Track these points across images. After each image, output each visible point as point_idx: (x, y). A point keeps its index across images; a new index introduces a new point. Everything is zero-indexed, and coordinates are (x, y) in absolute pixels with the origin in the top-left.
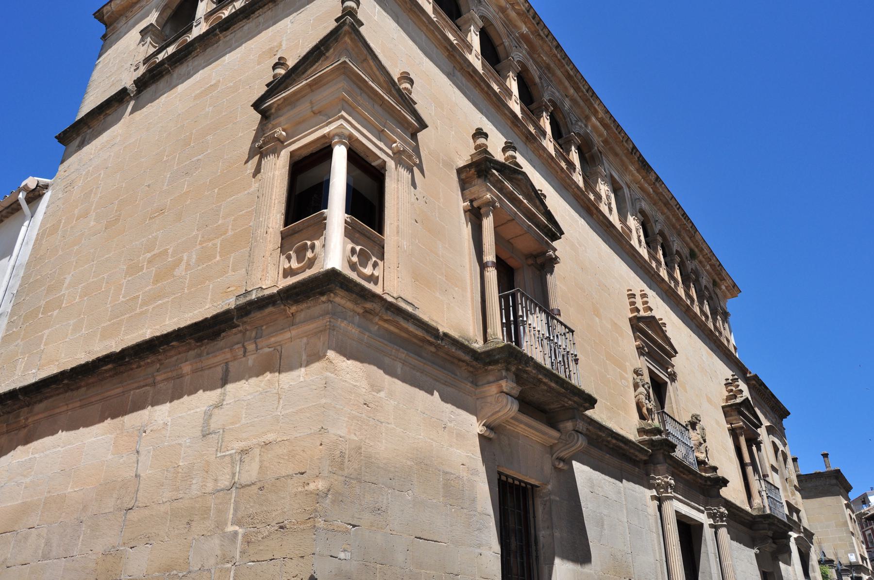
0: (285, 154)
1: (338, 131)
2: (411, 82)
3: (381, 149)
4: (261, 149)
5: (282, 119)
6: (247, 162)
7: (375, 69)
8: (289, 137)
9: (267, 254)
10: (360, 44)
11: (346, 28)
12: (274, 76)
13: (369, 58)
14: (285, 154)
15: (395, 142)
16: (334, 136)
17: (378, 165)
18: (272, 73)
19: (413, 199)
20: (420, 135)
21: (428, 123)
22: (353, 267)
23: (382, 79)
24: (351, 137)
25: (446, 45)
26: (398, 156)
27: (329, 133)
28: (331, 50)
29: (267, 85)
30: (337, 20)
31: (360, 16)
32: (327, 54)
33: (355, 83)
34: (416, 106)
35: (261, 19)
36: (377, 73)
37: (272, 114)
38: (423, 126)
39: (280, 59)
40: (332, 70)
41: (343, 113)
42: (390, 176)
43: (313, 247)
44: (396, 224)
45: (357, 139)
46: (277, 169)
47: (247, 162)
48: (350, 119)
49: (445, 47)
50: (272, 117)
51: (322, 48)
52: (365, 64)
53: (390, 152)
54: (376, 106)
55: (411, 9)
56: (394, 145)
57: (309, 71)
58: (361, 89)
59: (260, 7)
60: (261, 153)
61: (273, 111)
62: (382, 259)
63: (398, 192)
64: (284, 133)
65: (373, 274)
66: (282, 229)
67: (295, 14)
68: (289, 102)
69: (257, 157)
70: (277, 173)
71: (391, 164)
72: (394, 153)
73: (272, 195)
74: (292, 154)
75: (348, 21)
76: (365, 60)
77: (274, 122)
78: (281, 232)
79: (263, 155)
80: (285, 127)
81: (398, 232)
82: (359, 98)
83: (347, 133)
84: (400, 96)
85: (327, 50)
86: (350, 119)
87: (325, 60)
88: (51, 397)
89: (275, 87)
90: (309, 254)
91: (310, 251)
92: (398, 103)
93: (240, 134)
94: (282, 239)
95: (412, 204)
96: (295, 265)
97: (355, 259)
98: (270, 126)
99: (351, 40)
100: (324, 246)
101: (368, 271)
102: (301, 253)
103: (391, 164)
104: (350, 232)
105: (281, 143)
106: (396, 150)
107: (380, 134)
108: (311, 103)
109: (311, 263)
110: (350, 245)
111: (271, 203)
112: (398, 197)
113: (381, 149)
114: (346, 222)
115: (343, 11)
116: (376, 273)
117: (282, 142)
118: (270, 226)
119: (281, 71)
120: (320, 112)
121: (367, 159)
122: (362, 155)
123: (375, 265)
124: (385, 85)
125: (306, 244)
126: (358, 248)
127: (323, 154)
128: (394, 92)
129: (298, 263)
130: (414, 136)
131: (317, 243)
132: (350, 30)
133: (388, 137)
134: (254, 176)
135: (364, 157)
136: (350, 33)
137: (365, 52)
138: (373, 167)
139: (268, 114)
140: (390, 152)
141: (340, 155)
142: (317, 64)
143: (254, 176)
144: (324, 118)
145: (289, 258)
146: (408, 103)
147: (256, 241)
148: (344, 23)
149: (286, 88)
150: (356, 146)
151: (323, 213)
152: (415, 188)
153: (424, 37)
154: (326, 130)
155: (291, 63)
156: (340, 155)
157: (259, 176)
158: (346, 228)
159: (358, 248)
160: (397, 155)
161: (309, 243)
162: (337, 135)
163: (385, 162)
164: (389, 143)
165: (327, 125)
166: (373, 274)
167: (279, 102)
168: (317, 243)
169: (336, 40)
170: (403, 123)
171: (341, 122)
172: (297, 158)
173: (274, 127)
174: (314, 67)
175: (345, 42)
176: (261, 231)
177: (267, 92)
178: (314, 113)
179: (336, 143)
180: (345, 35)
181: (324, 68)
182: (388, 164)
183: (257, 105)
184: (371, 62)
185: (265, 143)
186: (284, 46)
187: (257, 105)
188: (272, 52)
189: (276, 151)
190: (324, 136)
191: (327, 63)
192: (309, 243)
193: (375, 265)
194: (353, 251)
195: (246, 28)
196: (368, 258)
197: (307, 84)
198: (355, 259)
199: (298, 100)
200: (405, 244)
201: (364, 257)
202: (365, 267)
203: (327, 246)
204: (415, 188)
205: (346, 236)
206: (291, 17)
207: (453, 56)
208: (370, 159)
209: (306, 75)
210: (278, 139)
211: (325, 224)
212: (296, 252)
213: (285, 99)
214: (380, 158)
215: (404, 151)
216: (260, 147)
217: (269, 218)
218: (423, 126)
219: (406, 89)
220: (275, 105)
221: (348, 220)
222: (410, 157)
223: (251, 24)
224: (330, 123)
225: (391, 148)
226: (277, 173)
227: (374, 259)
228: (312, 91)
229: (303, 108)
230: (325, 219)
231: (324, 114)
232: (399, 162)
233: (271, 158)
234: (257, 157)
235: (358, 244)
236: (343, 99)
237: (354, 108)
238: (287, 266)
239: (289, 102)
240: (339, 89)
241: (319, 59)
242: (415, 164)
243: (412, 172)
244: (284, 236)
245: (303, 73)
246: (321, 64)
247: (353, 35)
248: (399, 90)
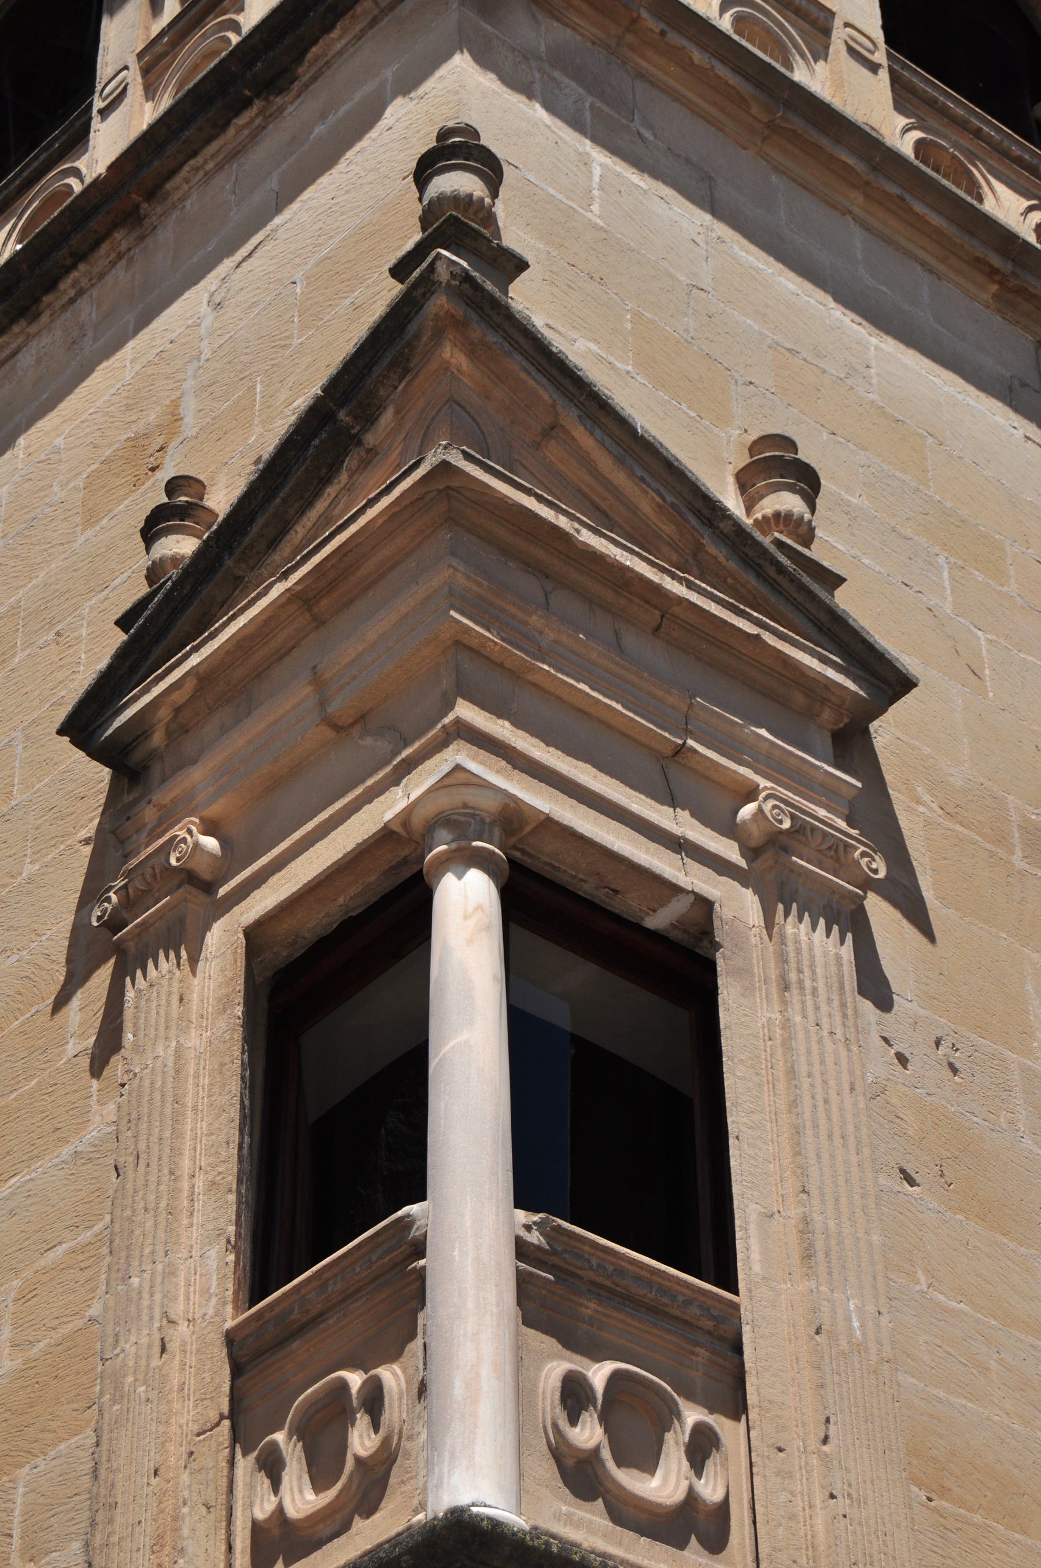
0: (223, 940)
1: (444, 801)
2: (807, 481)
3: (678, 845)
4: (123, 927)
5: (197, 775)
6: (61, 1001)
7: (605, 463)
8: (235, 853)
9: (175, 1455)
10: (516, 364)
11: (439, 303)
12: (153, 574)
13: (570, 418)
14: (223, 940)
15: (750, 794)
16: (431, 827)
17: (679, 924)
18: (143, 561)
19: (879, 1064)
20: (885, 732)
21: (909, 662)
22: (581, 1476)
23: (647, 503)
24: (512, 819)
25: (979, 250)
26: (773, 864)
27: (406, 817)
28: (387, 418)
29: (124, 623)
30: (399, 271)
31: (514, 236)
32: (370, 439)
33: (505, 551)
34: (843, 599)
35: (87, 310)
36: (620, 478)
37: (154, 755)
38: (890, 683)
39: (173, 486)
40: (392, 514)
41: (465, 711)
42: (743, 972)
43: (374, 1399)
44: (794, 1212)
45: (548, 823)
46: (196, 1012)
47: (61, 1001)
48: (502, 729)
49: (978, 262)
50: (156, 771)
51: (342, 415)
52: (553, 451)
53: (729, 850)
54: (631, 640)
55: (770, 125)
56: (747, 811)
57: (299, 531)
58: (543, 573)
59: (80, 257)
60: (119, 950)
61: (157, 739)
62: (736, 1406)
63: (787, 1043)
64: (210, 843)
65: (692, 1497)
66: (229, 1324)
67: (228, 263)
68: (227, 689)
69: (104, 974)
70: (194, 1041)
71: (738, 906)
72: (751, 852)
73: (176, 1152)
74: (255, 936)
75: (442, 273)
76: (552, 430)
77: (164, 796)
78: (230, 1339)
79: (130, 963)
80: (214, 810)
81: (808, 1255)
82: (535, 620)
83: (488, 804)
84: (747, 562)
85: (368, 417)
86: (502, 729)
87: (365, 464)
88: (361, 1557)
89: (155, 628)
90: (362, 1441)
91: (362, 1420)
92: (743, 599)
93: (29, 869)
94: (237, 1370)
95: (877, 1092)
96: (301, 1499)
97: (588, 1433)
98: (149, 814)
99: (472, 351)
100: (422, 1389)
101: (663, 1484)
102: (323, 1431)
103: (738, 906)
104: (548, 1297)
105: (202, 890)
106: (756, 836)
107: (668, 775)
108: (318, 681)
109: (372, 1484)
110: (556, 1366)
111: (174, 1193)
112: (792, 1072)
113: (678, 845)
114: (522, 1250)
115: (425, 221)
116: (710, 1490)
117: (209, 887)
118: (178, 1309)
119: (181, 546)
120: (362, 718)
121: (616, 905)
122: (587, 889)
123: (701, 1448)
124: (667, 529)
125: (343, 1386)
126: (599, 1375)
127: (392, 918)
128: (716, 551)
129: (317, 1489)
130: (851, 744)
131: (391, 1376)
132: (459, 310)
133: (708, 774)
134: (98, 1063)
135: (601, 896)
136: (460, 325)
137: (546, 393)
138: (654, 935)
139: (137, 755)
140: (729, 850)
141: (466, 908)
142: (331, 491)
143: (98, 1063)
144: (383, 745)
145: (272, 1467)
146: (794, 586)
147: (119, 1395)
148: (427, 285)
149: (202, 626)
150: (546, 855)
151: (406, 1224)
152: (884, 1001)
153: (858, 239)
154: (391, 806)
155: (220, 500)
156: (466, 908)
157: (116, 1066)
158: (522, 1281)
159: (599, 1375)
160: (766, 860)
161: (355, 1379)
162: (445, 820)
163: (705, 905)
164: (717, 804)
165: (396, 779)
166: (692, 1497)
167: (179, 697)
168: (391, 1376)
169: (403, 367)
170: (783, 695)
171: (460, 755)
172: (281, 954)
173: (168, 818)
174: (320, 506)
175: (446, 367)
176: (138, 1341)
177: (122, 655)
178: (338, 728)
179: (445, 863)
180: (438, 335)
181: (362, 506)
182: (724, 912)
183: (82, 726)
184: (584, 437)
185: (131, 903)
186: (190, 424)
187: (82, 726)
188: (142, 452)
189: (182, 937)
190: (386, 836)
191: (374, 480)
192: (355, 1379)
193: (701, 1448)
194: (574, 1395)
195: (26, 359)
196: (665, 1417)
197: (291, 597)
198: (588, 1433)
199: (260, 674)
200: (853, 1311)
201: (636, 1421)
202: (649, 1464)
203: (433, 1388)
204: (884, 1001)
205: (528, 1321)
206: (211, 282)
207: (1022, 292)
208: (630, 903)
209: (286, 548)
210: (188, 877)
211: (421, 1275)
212: (303, 1432)
213: (203, 677)
214: (676, 890)
215: (800, 829)
216: (113, 924)
217: (171, 1272)
218: (890, 683)
219: (782, 519)
220: (164, 713)
221: (534, 1238)
222: (836, 854)
223: (45, 340)
224: (409, 766)
225: (730, 829)
226: (194, 1041)
227: (692, 1415)
228: (319, 622)
229: (287, 707)
230: (419, 1249)
231: (383, 730)
232: (780, 892)
233: (163, 969)
234: (104, 974)
235: (596, 1353)
236: (460, 644)
237: (516, 675)
238: (264, 1508)
239: (227, 689)
240: (432, 603)
241: (334, 468)
242: (868, 884)
243: (855, 924)
244: (248, 1356)
245: (273, 543)
246: (349, 488)
247: (478, 331)
248: (737, 538)
